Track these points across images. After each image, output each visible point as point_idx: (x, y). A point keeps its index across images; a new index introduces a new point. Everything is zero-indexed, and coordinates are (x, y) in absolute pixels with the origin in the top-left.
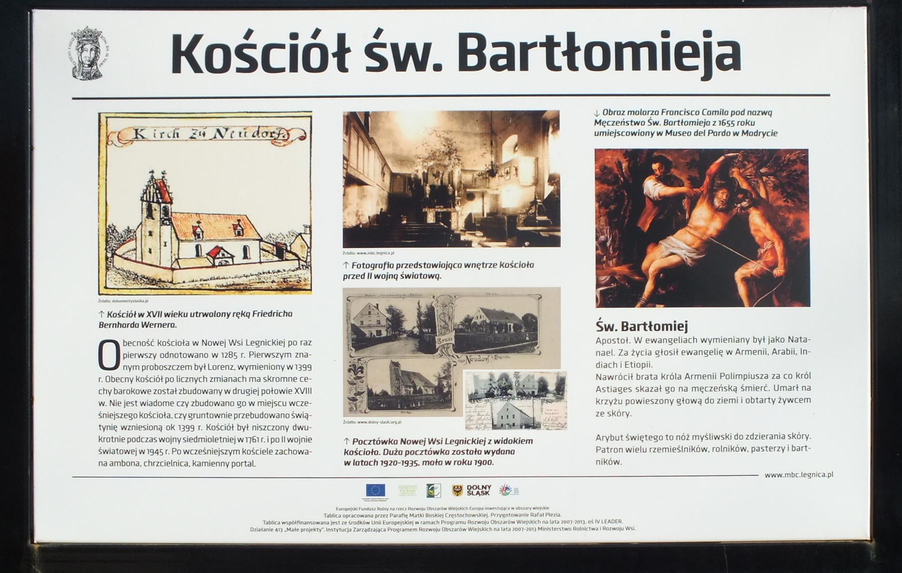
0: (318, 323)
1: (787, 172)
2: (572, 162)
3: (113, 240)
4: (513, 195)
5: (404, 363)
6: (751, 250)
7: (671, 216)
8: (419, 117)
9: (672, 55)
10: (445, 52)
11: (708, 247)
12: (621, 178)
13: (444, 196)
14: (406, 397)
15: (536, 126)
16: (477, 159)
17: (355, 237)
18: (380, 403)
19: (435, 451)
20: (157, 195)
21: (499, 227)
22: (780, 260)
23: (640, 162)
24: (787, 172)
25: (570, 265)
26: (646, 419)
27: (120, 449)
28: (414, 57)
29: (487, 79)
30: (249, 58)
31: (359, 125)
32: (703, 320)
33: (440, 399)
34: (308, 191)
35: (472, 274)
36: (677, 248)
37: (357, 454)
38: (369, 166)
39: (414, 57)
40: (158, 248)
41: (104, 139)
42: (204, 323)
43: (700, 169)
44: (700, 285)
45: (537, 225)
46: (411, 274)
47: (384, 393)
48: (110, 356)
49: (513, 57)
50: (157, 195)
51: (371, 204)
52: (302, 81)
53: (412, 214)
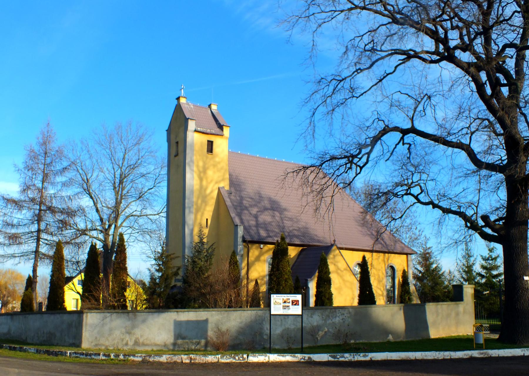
0: (281, 306)
1: (298, 301)
2: (291, 301)
5: (285, 307)
12: (292, 301)
22: (336, 360)
24: (298, 301)
27: (274, 310)
34: (281, 301)
35: (287, 304)
42: (277, 306)
43: (295, 301)
44: (295, 305)
45: (289, 303)
46: (285, 304)
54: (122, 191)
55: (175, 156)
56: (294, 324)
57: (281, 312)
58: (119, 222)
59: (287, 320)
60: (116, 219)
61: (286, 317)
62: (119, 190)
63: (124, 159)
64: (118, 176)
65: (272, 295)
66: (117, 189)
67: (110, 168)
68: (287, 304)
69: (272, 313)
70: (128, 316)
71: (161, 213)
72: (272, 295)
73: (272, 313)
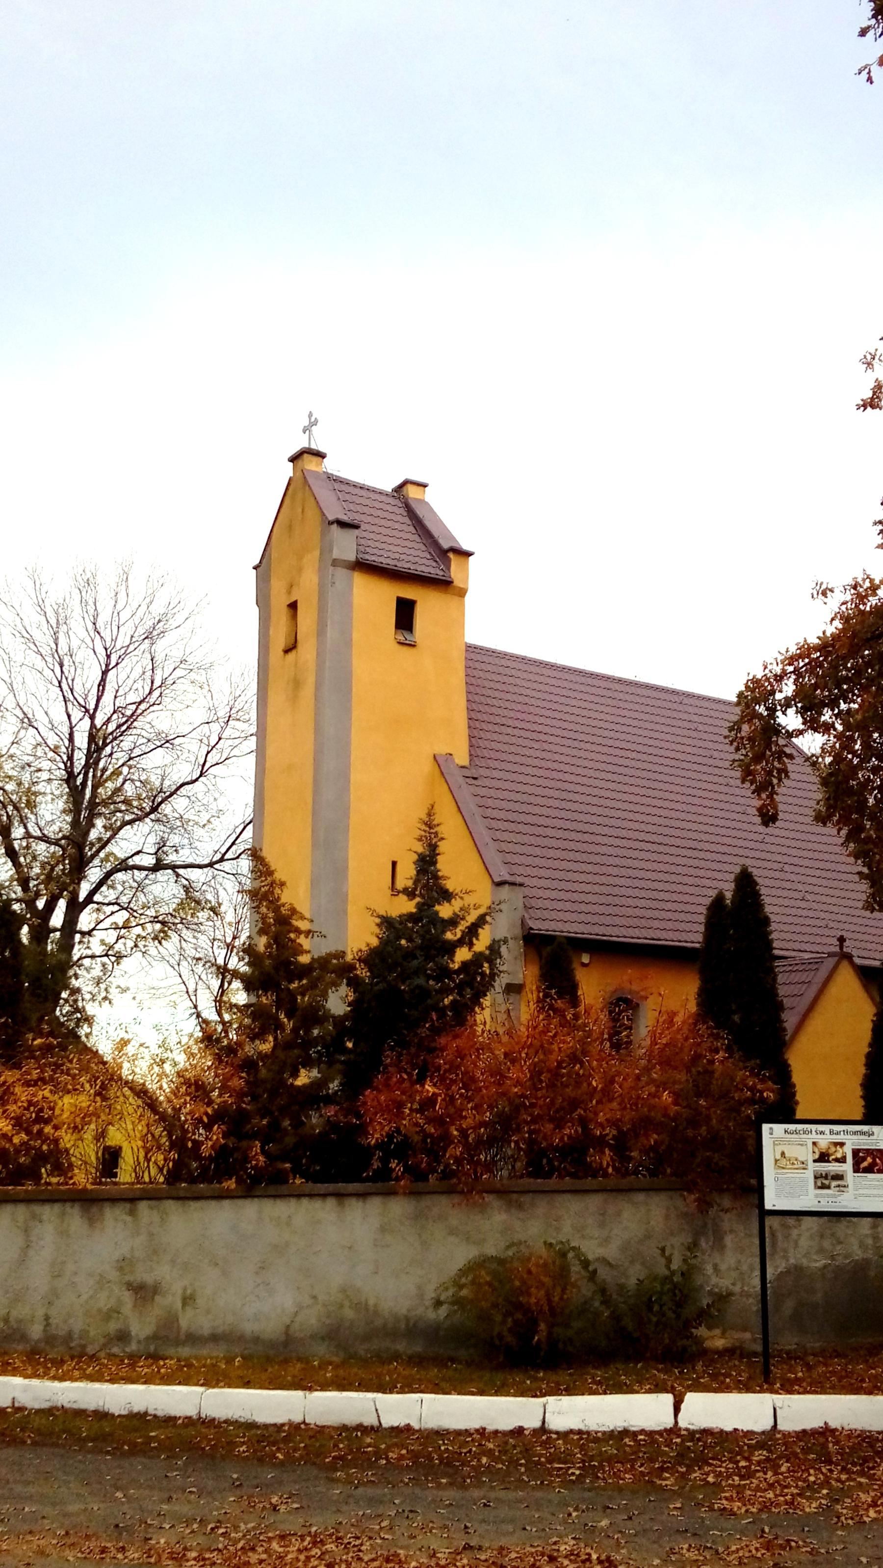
0: (809, 1175)
2: (848, 1150)
3: (776, 1161)
4: (839, 1155)
5: (823, 1181)
6: (877, 1165)
7: (864, 1159)
8: (824, 1142)
9: (862, 1133)
10: (827, 1132)
11: (870, 1164)
12: (855, 1153)
13: (828, 1155)
14: (824, 1187)
15: (842, 1144)
16: (833, 1149)
17: (815, 1161)
18: (820, 1188)
19: (828, 1196)
20: (783, 1154)
21: (837, 1160)
23: (859, 1150)
25: (847, 1167)
26: (861, 1192)
28: (822, 1133)
29: (834, 1136)
30: (796, 1132)
31: (814, 1144)
32: (870, 1176)
33: (829, 1187)
34: (807, 1154)
35: (832, 1167)
36: (865, 1164)
37: (817, 1196)
38: (816, 1150)
39: (822, 1133)
40: (783, 1162)
41: (774, 1144)
43: (869, 1152)
45: (843, 1160)
47: (348, 985)
48: (776, 1180)
49: (838, 1133)
50: (783, 1154)
51: (817, 1156)
52: (805, 1136)
53: (823, 1157)
54: (95, 788)
55: (287, 651)
56: (821, 1250)
57: (809, 1199)
58: (84, 889)
59: (795, 1232)
60: (79, 866)
61: (791, 1221)
62: (84, 784)
63: (102, 683)
64: (82, 740)
65: (766, 1127)
66: (79, 781)
67: (59, 717)
68: (832, 1167)
69: (768, 1206)
70: (132, 1213)
71: (222, 860)
72: (766, 1127)
73: (768, 1206)
